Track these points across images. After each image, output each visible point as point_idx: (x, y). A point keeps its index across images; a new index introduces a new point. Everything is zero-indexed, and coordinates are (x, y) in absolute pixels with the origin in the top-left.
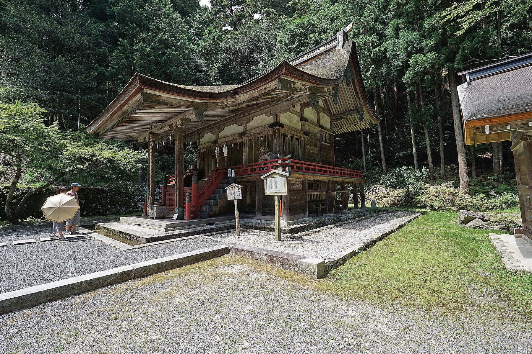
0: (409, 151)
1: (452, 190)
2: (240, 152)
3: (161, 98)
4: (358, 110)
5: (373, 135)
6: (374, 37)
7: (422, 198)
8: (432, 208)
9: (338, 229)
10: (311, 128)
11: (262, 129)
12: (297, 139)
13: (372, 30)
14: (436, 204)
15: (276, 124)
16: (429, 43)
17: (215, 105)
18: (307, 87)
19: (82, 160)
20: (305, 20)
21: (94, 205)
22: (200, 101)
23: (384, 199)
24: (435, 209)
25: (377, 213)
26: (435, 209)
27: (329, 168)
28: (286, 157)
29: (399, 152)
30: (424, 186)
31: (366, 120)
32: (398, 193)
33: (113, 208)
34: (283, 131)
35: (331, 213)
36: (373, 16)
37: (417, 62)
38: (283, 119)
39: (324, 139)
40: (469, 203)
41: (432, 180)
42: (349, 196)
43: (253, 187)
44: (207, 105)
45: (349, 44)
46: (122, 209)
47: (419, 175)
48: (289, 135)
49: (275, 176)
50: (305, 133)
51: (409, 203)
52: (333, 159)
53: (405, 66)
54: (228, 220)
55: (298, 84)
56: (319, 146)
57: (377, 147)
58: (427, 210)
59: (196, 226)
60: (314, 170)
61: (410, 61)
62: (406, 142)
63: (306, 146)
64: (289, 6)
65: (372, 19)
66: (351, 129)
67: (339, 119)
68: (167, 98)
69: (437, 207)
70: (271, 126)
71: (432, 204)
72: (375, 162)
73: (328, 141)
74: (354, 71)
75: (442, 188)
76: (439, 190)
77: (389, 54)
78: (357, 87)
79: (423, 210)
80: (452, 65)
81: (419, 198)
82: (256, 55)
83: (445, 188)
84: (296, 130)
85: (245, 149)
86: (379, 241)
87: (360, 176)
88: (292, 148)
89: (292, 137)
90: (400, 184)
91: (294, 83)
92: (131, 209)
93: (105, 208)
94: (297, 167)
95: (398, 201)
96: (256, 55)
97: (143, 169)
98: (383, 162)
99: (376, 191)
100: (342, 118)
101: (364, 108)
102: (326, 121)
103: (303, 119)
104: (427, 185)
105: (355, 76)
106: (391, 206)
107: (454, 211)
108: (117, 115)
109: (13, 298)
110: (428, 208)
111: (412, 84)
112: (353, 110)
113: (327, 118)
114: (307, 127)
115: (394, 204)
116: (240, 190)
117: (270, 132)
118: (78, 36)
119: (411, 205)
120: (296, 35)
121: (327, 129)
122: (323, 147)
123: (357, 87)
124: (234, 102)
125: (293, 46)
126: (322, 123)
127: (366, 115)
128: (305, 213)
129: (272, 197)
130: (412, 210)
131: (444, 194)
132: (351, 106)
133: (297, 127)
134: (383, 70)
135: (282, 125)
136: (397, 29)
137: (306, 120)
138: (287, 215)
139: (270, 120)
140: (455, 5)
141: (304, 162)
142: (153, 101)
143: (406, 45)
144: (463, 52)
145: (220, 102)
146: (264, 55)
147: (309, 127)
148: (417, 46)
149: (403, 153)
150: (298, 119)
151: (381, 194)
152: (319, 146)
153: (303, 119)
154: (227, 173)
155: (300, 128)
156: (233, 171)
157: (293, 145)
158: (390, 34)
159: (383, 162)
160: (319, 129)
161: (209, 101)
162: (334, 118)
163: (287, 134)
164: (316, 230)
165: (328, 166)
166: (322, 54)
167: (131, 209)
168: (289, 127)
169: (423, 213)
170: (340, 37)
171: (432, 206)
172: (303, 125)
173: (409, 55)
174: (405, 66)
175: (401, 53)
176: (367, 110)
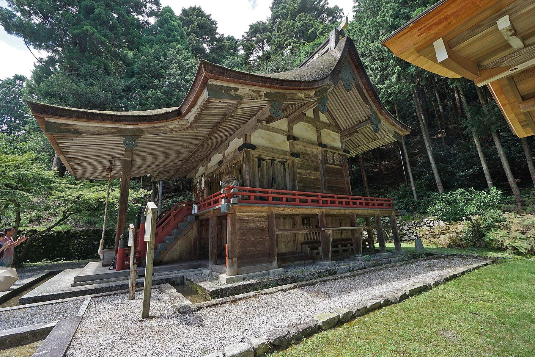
0: (476, 168)
3: (74, 127)
8: (516, 251)
9: (299, 292)
10: (308, 149)
12: (283, 163)
14: (523, 246)
15: (248, 146)
17: (155, 130)
18: (263, 94)
22: (128, 127)
23: (442, 237)
24: (521, 254)
25: (420, 256)
26: (521, 254)
27: (338, 198)
29: (463, 171)
30: (502, 217)
32: (462, 228)
34: (255, 153)
35: (327, 260)
36: (391, 12)
39: (330, 160)
41: (519, 207)
42: (361, 233)
44: (142, 131)
45: (343, 41)
47: (486, 201)
48: (268, 159)
50: (294, 154)
51: (477, 242)
52: (348, 185)
55: (244, 90)
56: (321, 169)
58: (506, 255)
59: (121, 278)
60: (361, 204)
62: (473, 156)
63: (298, 171)
64: (310, 33)
65: (391, 16)
67: (350, 134)
68: (81, 126)
69: (524, 251)
71: (515, 245)
73: (337, 162)
74: (356, 72)
76: (527, 222)
78: (365, 92)
79: (499, 255)
81: (491, 235)
84: (284, 153)
86: (331, 328)
87: (389, 205)
88: (274, 174)
89: (273, 160)
90: (455, 216)
91: (236, 90)
94: (287, 199)
95: (461, 239)
97: (140, 208)
99: (431, 224)
100: (354, 132)
101: (380, 116)
102: (333, 139)
103: (291, 137)
104: (507, 215)
105: (359, 78)
106: (450, 246)
112: (366, 120)
113: (336, 136)
114: (299, 147)
115: (454, 245)
118: (102, 93)
119: (480, 246)
121: (338, 149)
122: (329, 171)
123: (365, 92)
124: (184, 125)
126: (326, 140)
128: (271, 263)
130: (480, 254)
132: (362, 116)
133: (285, 149)
135: (254, 147)
137: (295, 138)
138: (231, 266)
141: (270, 190)
142: (61, 131)
145: (162, 127)
147: (303, 148)
149: (467, 172)
150: (285, 138)
151: (434, 230)
152: (321, 169)
153: (291, 137)
155: (288, 149)
157: (274, 170)
160: (320, 149)
161: (142, 126)
162: (344, 133)
163: (263, 157)
164: (253, 293)
165: (336, 196)
168: (265, 148)
169: (495, 261)
171: (514, 248)
172: (292, 145)
176: (386, 118)
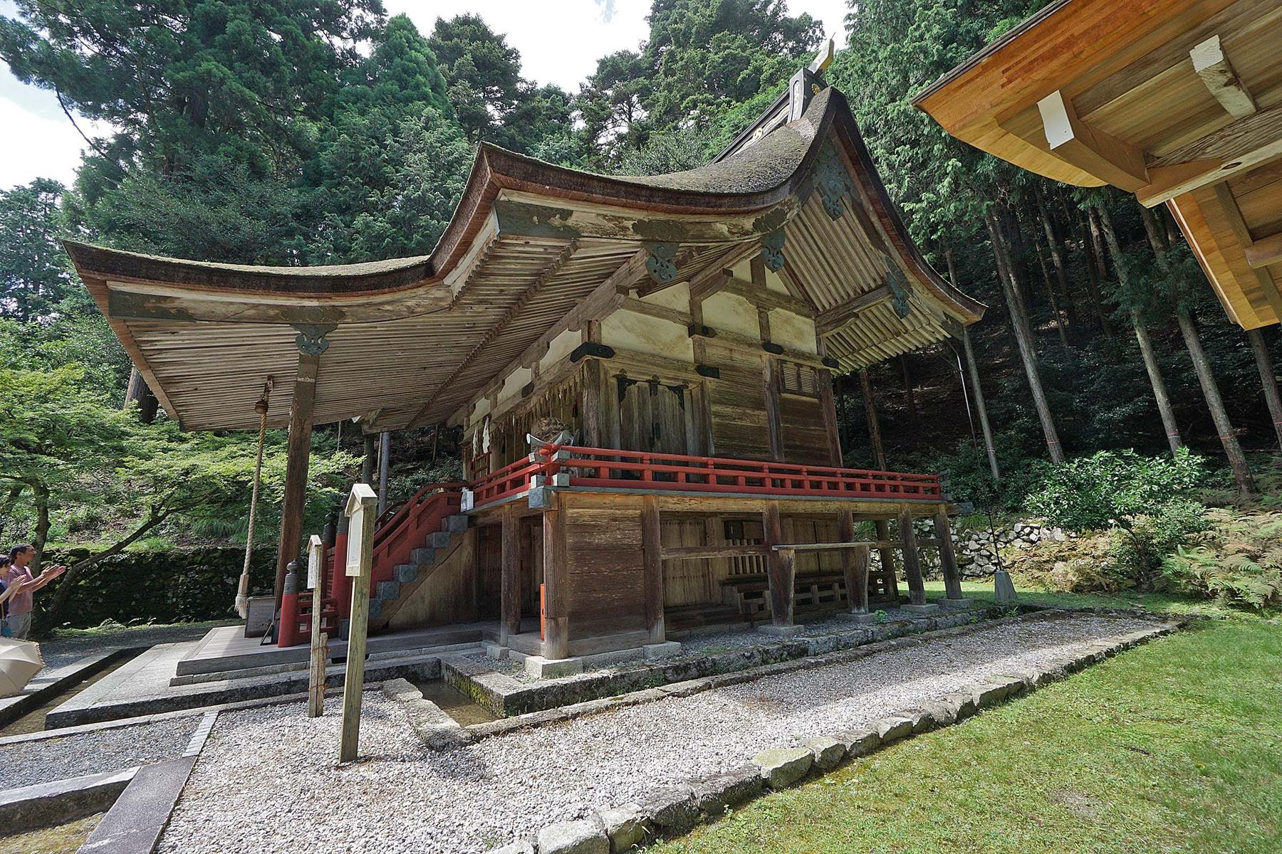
0: (1140, 402)
3: (176, 304)
8: (1236, 600)
9: (717, 697)
10: (737, 356)
12: (678, 390)
14: (1254, 588)
15: (594, 349)
17: (371, 311)
18: (629, 224)
22: (307, 303)
23: (1059, 566)
24: (1248, 607)
25: (1007, 613)
26: (1248, 607)
27: (810, 473)
29: (1109, 409)
30: (1202, 519)
32: (1106, 544)
34: (610, 367)
35: (783, 621)
36: (936, 29)
39: (791, 384)
41: (1245, 496)
42: (865, 557)
44: (339, 314)
45: (822, 98)
47: (1165, 480)
48: (642, 380)
50: (704, 369)
51: (1143, 580)
52: (834, 442)
55: (584, 215)
56: (769, 404)
58: (1213, 610)
59: (291, 666)
62: (1133, 374)
63: (714, 408)
64: (744, 79)
65: (936, 39)
67: (840, 321)
68: (195, 301)
69: (1255, 600)
71: (1235, 585)
73: (807, 389)
74: (853, 172)
76: (1264, 531)
78: (874, 219)
79: (1197, 609)
81: (1177, 561)
84: (681, 365)
86: (793, 784)
87: (933, 490)
88: (656, 416)
89: (654, 384)
90: (1090, 517)
91: (566, 214)
94: (687, 475)
95: (1104, 573)
97: (336, 498)
99: (1033, 537)
100: (848, 316)
101: (911, 278)
102: (797, 332)
103: (698, 329)
104: (1215, 514)
105: (860, 187)
106: (1077, 589)
112: (878, 287)
113: (806, 325)
114: (716, 352)
115: (1087, 585)
118: (244, 222)
119: (1151, 589)
121: (809, 357)
122: (788, 410)
123: (874, 219)
124: (441, 299)
126: (780, 335)
128: (649, 628)
130: (1150, 608)
132: (868, 279)
133: (682, 357)
135: (608, 352)
137: (707, 331)
138: (555, 636)
141: (647, 455)
142: (145, 314)
145: (388, 303)
147: (726, 353)
149: (1120, 412)
150: (684, 330)
151: (1039, 550)
152: (769, 404)
153: (698, 329)
155: (689, 355)
157: (656, 408)
160: (766, 355)
161: (339, 302)
162: (825, 319)
163: (630, 376)
164: (606, 701)
165: (804, 468)
168: (635, 355)
169: (1185, 624)
171: (1232, 593)
172: (699, 347)
176: (925, 283)
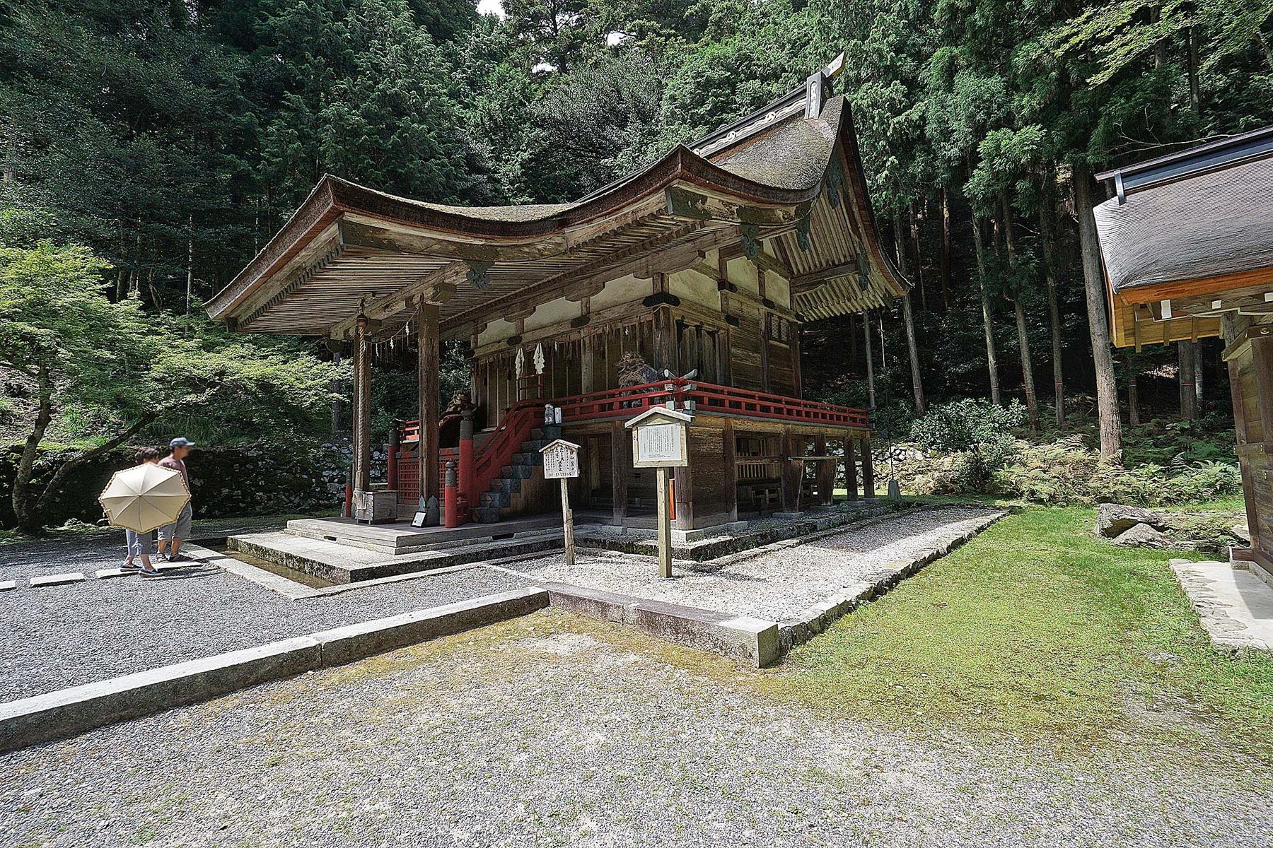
0: (978, 362)
1: (1080, 454)
2: (575, 364)
3: (386, 236)
4: (856, 263)
5: (894, 323)
6: (896, 90)
7: (1009, 474)
8: (1034, 497)
9: (810, 548)
10: (744, 307)
11: (626, 310)
12: (711, 334)
13: (891, 73)
14: (1044, 490)
15: (661, 298)
16: (1027, 102)
17: (515, 252)
18: (734, 209)
19: (196, 384)
20: (729, 48)
21: (225, 491)
22: (477, 242)
23: (919, 478)
24: (1041, 501)
25: (902, 510)
26: (1041, 501)
27: (787, 403)
28: (685, 377)
29: (956, 365)
30: (1014, 446)
31: (877, 287)
32: (953, 463)
33: (269, 499)
34: (676, 314)
35: (792, 510)
36: (892, 38)
37: (998, 147)
38: (677, 284)
39: (775, 334)
40: (1122, 487)
41: (1033, 432)
42: (835, 470)
43: (605, 448)
44: (494, 252)
45: (835, 105)
46: (291, 501)
47: (1003, 420)
48: (692, 325)
49: (659, 421)
50: (731, 319)
51: (979, 487)
52: (797, 381)
53: (970, 159)
54: (545, 526)
55: (714, 201)
56: (762, 349)
57: (903, 352)
58: (1021, 503)
59: (468, 541)
61: (982, 147)
62: (972, 339)
63: (733, 350)
64: (691, 14)
65: (890, 45)
66: (839, 309)
67: (812, 285)
68: (399, 234)
69: (1045, 497)
70: (648, 301)
71: (1035, 488)
72: (897, 388)
73: (784, 338)
74: (847, 170)
75: (1057, 449)
76: (1050, 455)
77: (931, 129)
78: (855, 210)
79: (1012, 503)
80: (1083, 155)
81: (1002, 474)
82: (612, 133)
83: (1064, 450)
84: (709, 312)
85: (587, 358)
86: (908, 576)
87: (863, 421)
88: (700, 356)
89: (699, 328)
90: (958, 440)
91: (704, 199)
92: (314, 501)
93: (252, 498)
94: (710, 399)
95: (952, 482)
96: (612, 133)
97: (341, 404)
98: (917, 387)
99: (901, 457)
100: (820, 283)
101: (871, 260)
102: (779, 289)
103: (724, 284)
104: (1022, 444)
105: (850, 182)
106: (936, 492)
107: (1087, 507)
108: (280, 275)
109: (31, 715)
110: (1024, 498)
111: (987, 201)
112: (846, 263)
113: (783, 283)
114: (733, 305)
115: (943, 489)
116: (574, 455)
117: (647, 315)
118: (186, 86)
119: (983, 492)
120: (709, 83)
121: (782, 310)
122: (773, 353)
123: (855, 210)
124: (559, 245)
125: (702, 111)
126: (771, 294)
127: (876, 276)
128: (729, 511)
129: (651, 473)
130: (986, 503)
131: (1062, 464)
132: (840, 255)
133: (711, 305)
134: (917, 167)
135: (675, 301)
136: (950, 71)
137: (732, 287)
138: (686, 515)
139: (645, 286)
140: (1088, 12)
141: (726, 389)
142: (366, 243)
143: (972, 108)
144: (1107, 124)
145: (526, 245)
146: (633, 132)
147: (739, 305)
148: (999, 109)
149: (963, 368)
150: (714, 284)
151: (912, 465)
152: (762, 349)
153: (724, 284)
154: (542, 415)
155: (718, 306)
156: (558, 410)
157: (700, 348)
158: (932, 82)
159: (917, 387)
160: (764, 309)
161: (500, 242)
162: (799, 282)
163: (686, 321)
164: (756, 550)
165: (784, 398)
166: (769, 129)
167: (314, 501)
168: (692, 305)
169: (1012, 510)
170: (814, 88)
171: (1033, 493)
172: (725, 299)
173: (980, 131)
174: (970, 159)
175: (960, 127)
176: (879, 264)
